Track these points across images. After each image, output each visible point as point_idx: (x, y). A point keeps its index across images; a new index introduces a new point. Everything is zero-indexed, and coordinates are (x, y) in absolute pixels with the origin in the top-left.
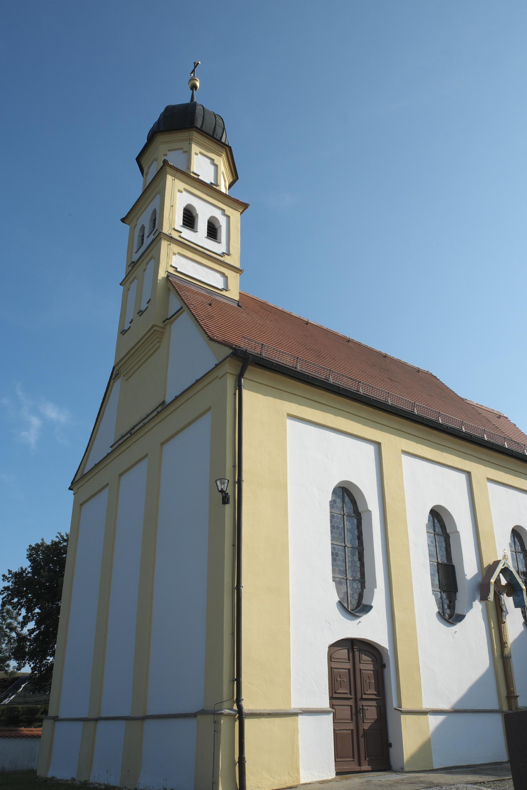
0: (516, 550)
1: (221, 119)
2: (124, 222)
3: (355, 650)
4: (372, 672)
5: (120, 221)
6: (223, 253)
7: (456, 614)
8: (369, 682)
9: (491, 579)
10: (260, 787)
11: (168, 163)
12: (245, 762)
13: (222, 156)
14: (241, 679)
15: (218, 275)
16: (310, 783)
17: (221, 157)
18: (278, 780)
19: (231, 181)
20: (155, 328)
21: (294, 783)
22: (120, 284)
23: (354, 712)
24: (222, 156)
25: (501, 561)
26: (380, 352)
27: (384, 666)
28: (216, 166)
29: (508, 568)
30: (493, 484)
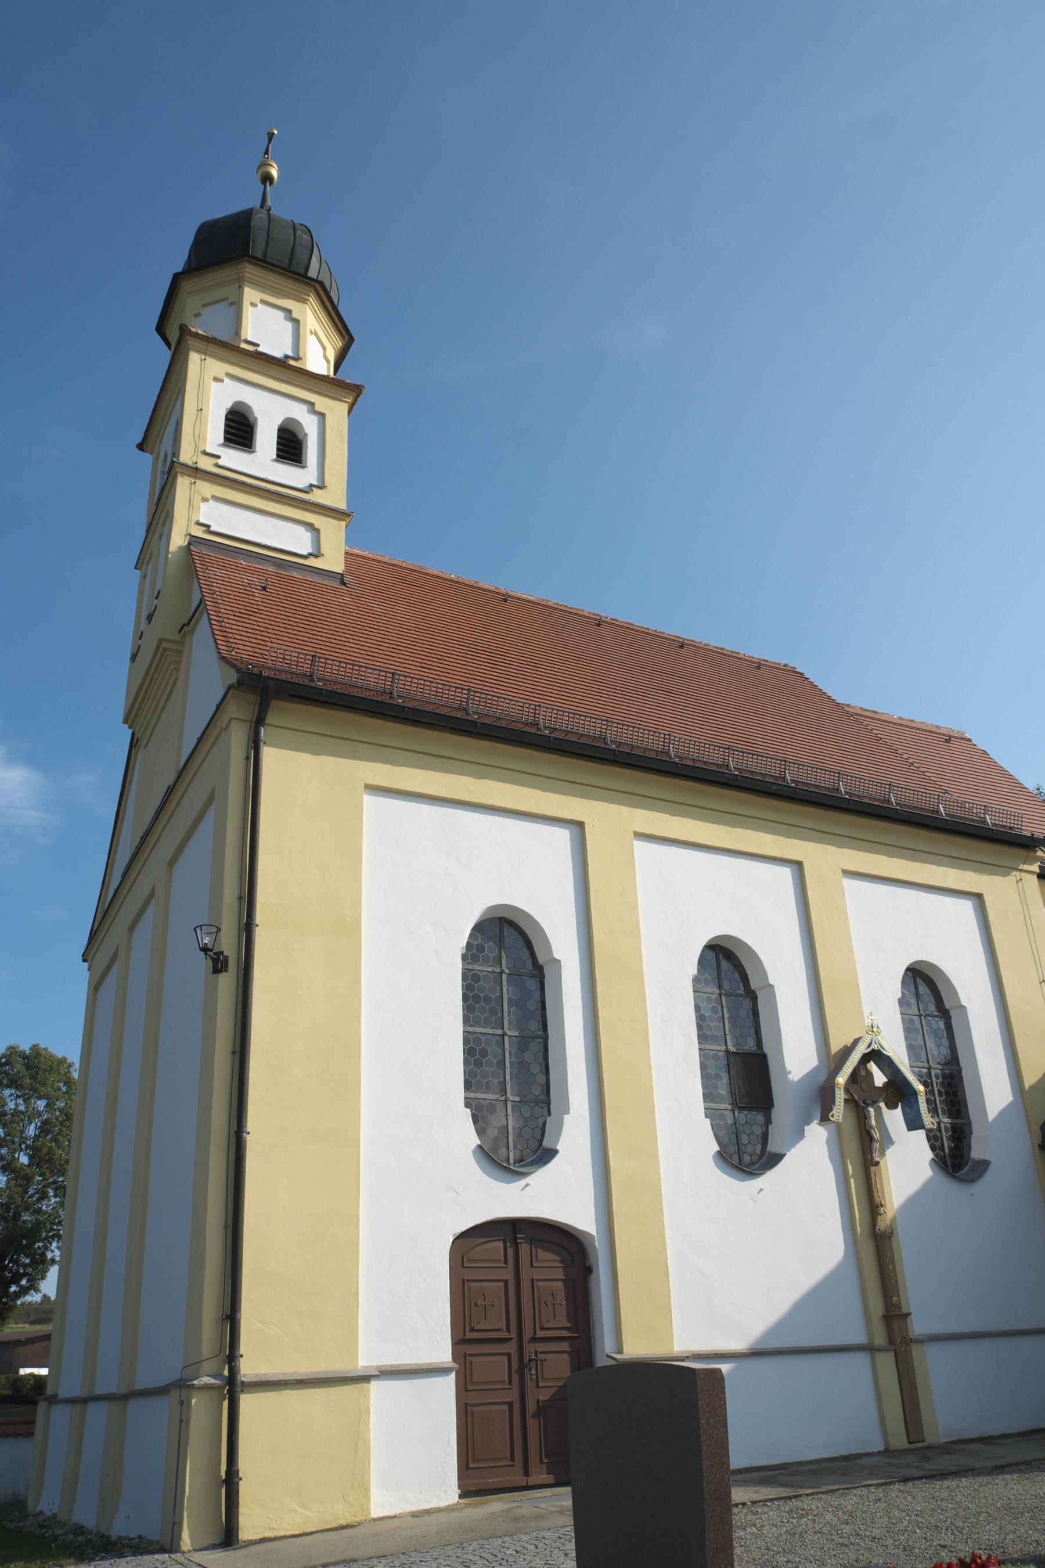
0: (922, 1012)
1: (308, 232)
2: (143, 450)
3: (518, 1241)
4: (560, 1284)
5: (136, 448)
6: (311, 486)
7: (770, 1153)
8: (554, 1305)
9: (836, 1077)
10: (275, 1529)
11: (190, 329)
12: (237, 1479)
13: (309, 303)
14: (238, 1315)
15: (301, 530)
16: (395, 1515)
17: (307, 303)
18: (319, 1512)
19: (339, 346)
20: (164, 645)
21: (355, 1517)
22: (135, 568)
23: (515, 1366)
24: (309, 303)
25: (863, 1038)
26: (676, 637)
27: (588, 1270)
28: (296, 322)
29: (879, 1051)
30: (860, 882)
